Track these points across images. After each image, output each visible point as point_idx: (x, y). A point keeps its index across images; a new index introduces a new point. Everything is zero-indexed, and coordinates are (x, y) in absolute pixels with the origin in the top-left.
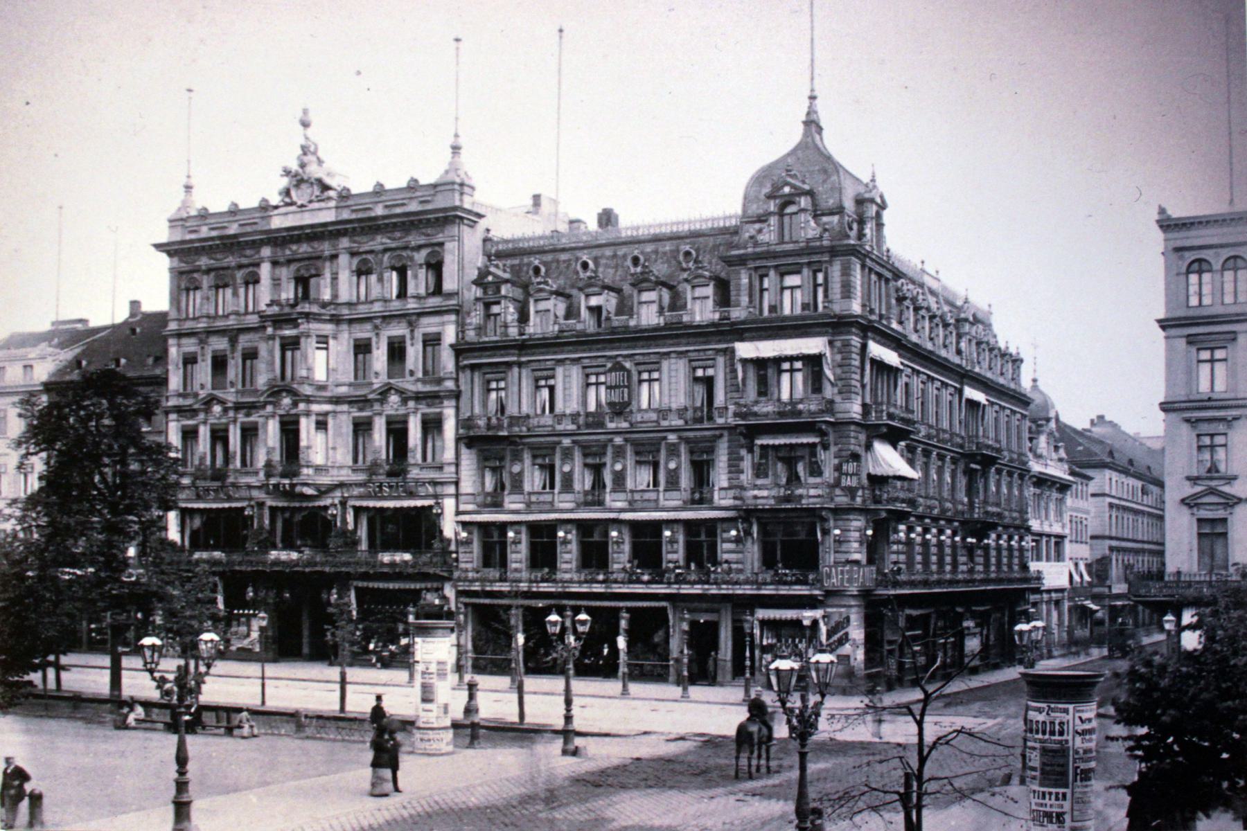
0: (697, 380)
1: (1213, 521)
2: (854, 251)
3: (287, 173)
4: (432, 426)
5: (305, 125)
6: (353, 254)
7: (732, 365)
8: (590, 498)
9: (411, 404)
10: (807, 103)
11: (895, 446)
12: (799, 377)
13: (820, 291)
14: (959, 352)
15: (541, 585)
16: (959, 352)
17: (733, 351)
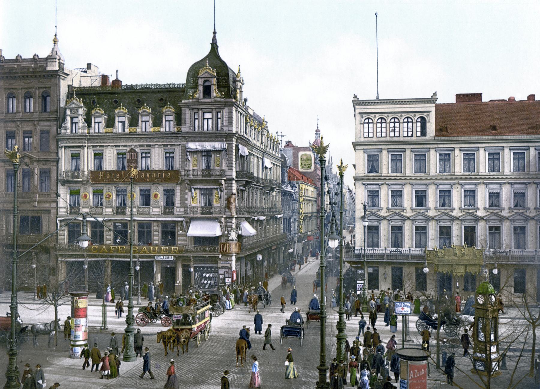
10: (212, 35)
13: (219, 121)
14: (262, 143)
16: (262, 143)
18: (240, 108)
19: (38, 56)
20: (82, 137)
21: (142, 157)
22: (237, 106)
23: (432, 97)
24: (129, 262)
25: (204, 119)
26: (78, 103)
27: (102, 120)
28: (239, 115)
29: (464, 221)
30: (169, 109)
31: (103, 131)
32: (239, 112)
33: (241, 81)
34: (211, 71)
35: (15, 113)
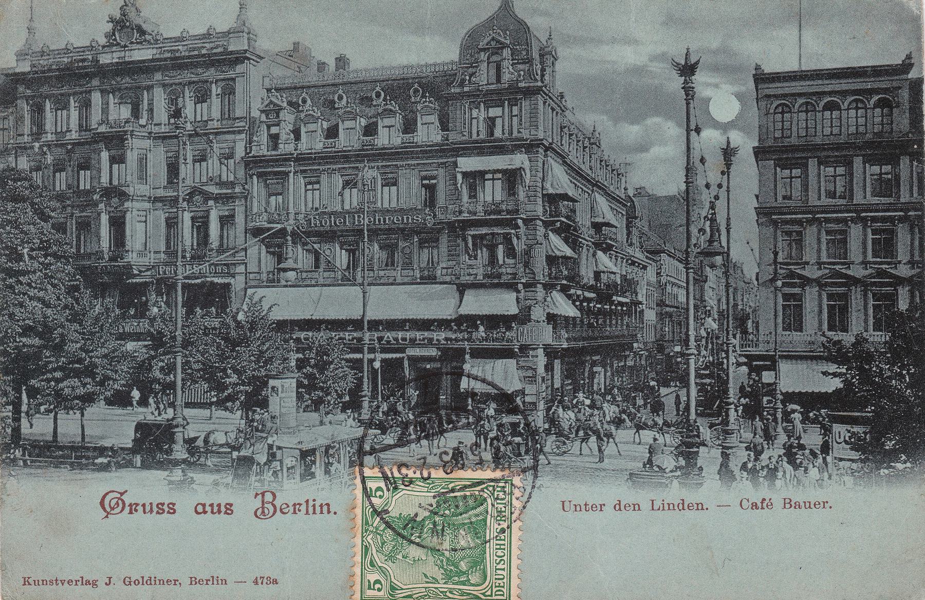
0: (423, 185)
2: (537, 91)
4: (226, 221)
5: (748, 243)
6: (164, 86)
7: (455, 178)
8: (426, 273)
9: (211, 203)
11: (560, 235)
12: (498, 184)
13: (515, 119)
17: (455, 164)
18: (550, 98)
19: (188, 32)
20: (285, 159)
22: (547, 95)
23: (903, 61)
24: (361, 360)
26: (279, 103)
27: (397, 121)
28: (550, 110)
29: (826, 285)
30: (427, 104)
31: (319, 146)
32: (549, 105)
33: (553, 53)
34: (501, 36)
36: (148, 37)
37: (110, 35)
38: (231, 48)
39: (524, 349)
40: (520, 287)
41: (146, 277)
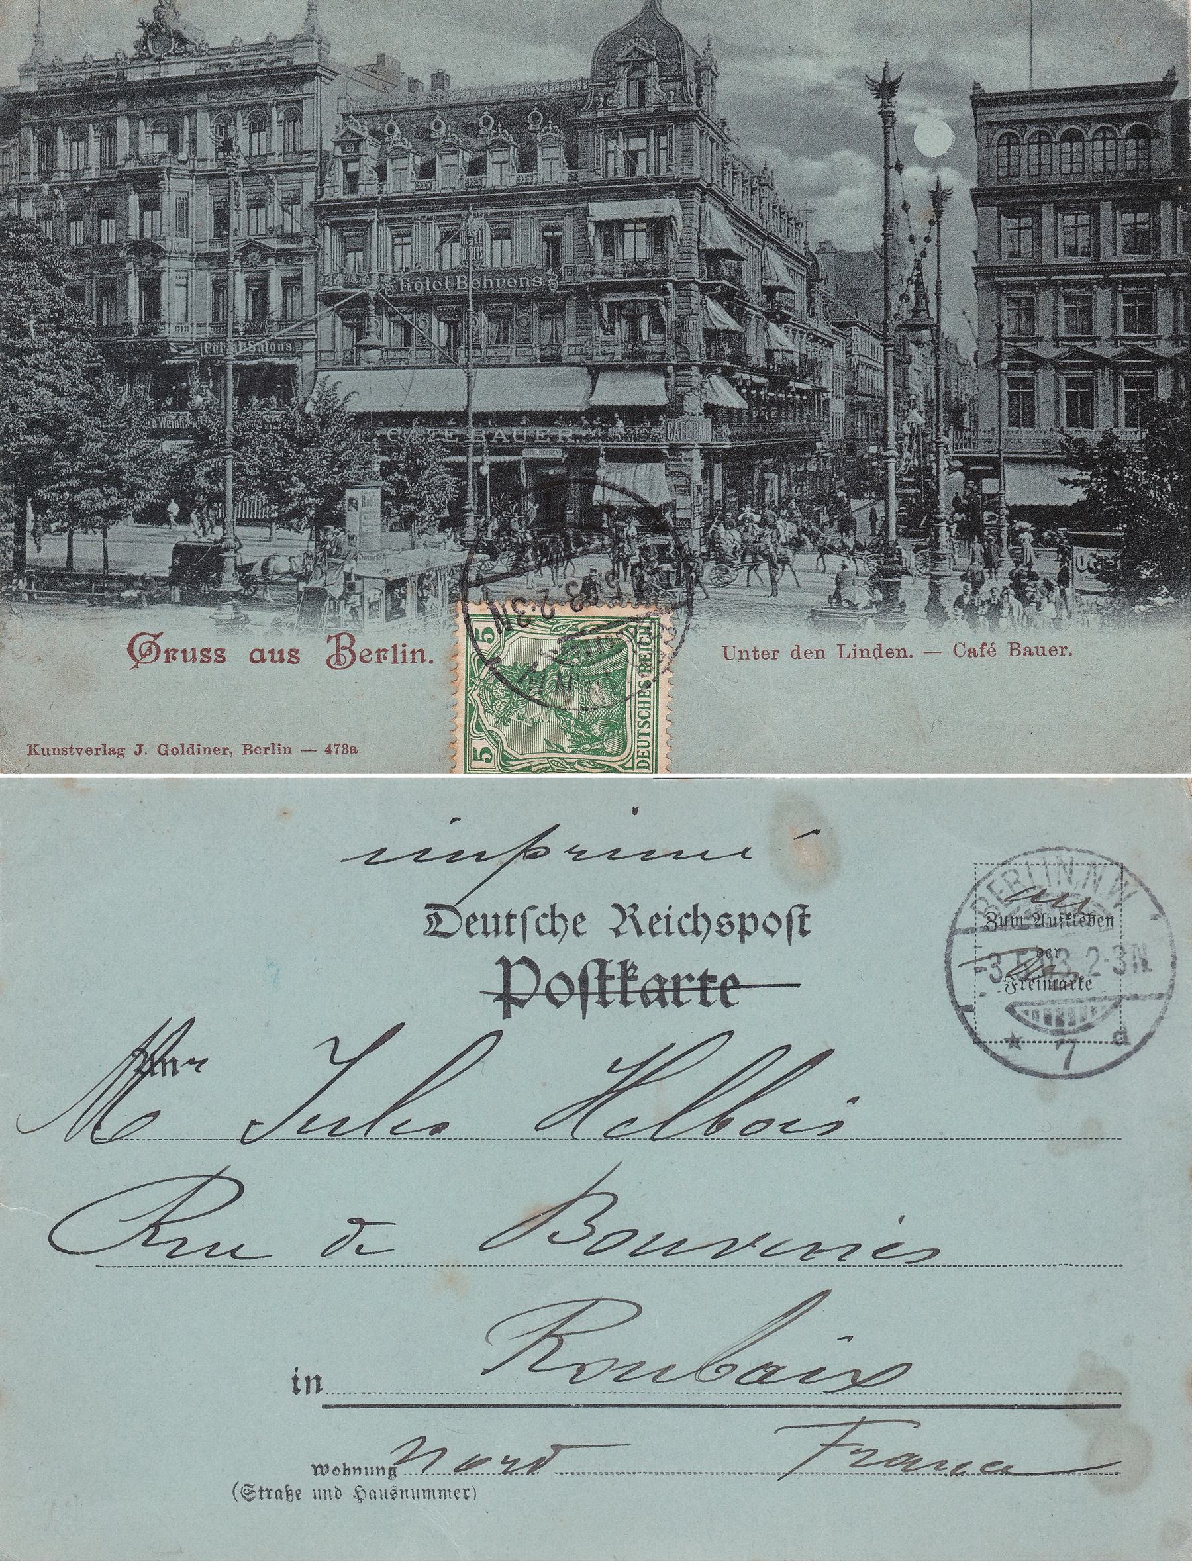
0: (545, 239)
1: (1022, 380)
2: (691, 117)
3: (143, 25)
4: (291, 284)
13: (663, 154)
15: (1133, 260)
17: (586, 211)
18: (709, 125)
19: (241, 41)
20: (367, 205)
21: (394, 245)
23: (1164, 78)
24: (465, 464)
25: (659, 149)
26: (360, 133)
30: (550, 133)
31: (410, 188)
32: (707, 135)
33: (713, 68)
35: (265, 156)
36: (189, 47)
37: (140, 45)
38: (297, 61)
39: (675, 449)
40: (670, 369)
41: (187, 358)
